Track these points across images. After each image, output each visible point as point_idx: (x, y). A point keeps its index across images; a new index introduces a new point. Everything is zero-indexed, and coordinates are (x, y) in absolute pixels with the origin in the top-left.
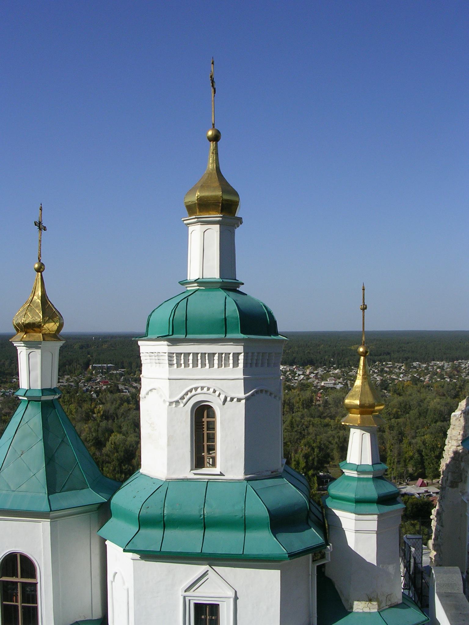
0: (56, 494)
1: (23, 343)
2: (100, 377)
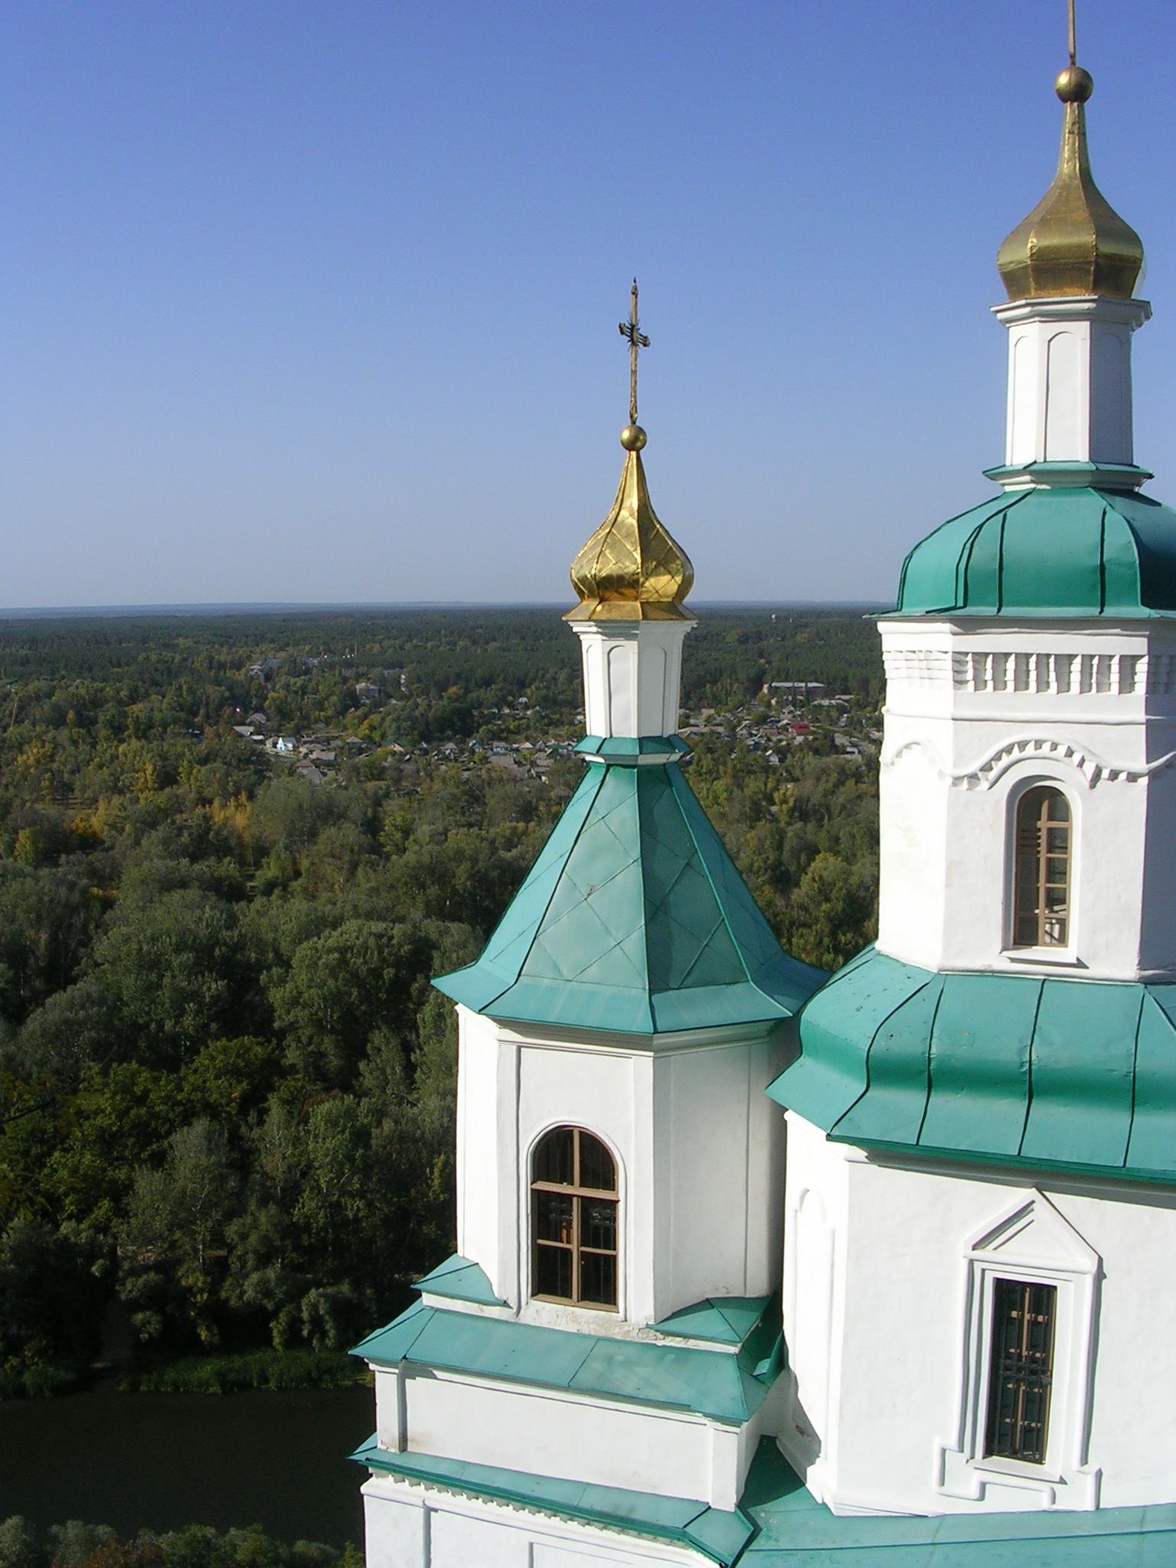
0: (671, 992)
1: (596, 626)
2: (789, 713)
